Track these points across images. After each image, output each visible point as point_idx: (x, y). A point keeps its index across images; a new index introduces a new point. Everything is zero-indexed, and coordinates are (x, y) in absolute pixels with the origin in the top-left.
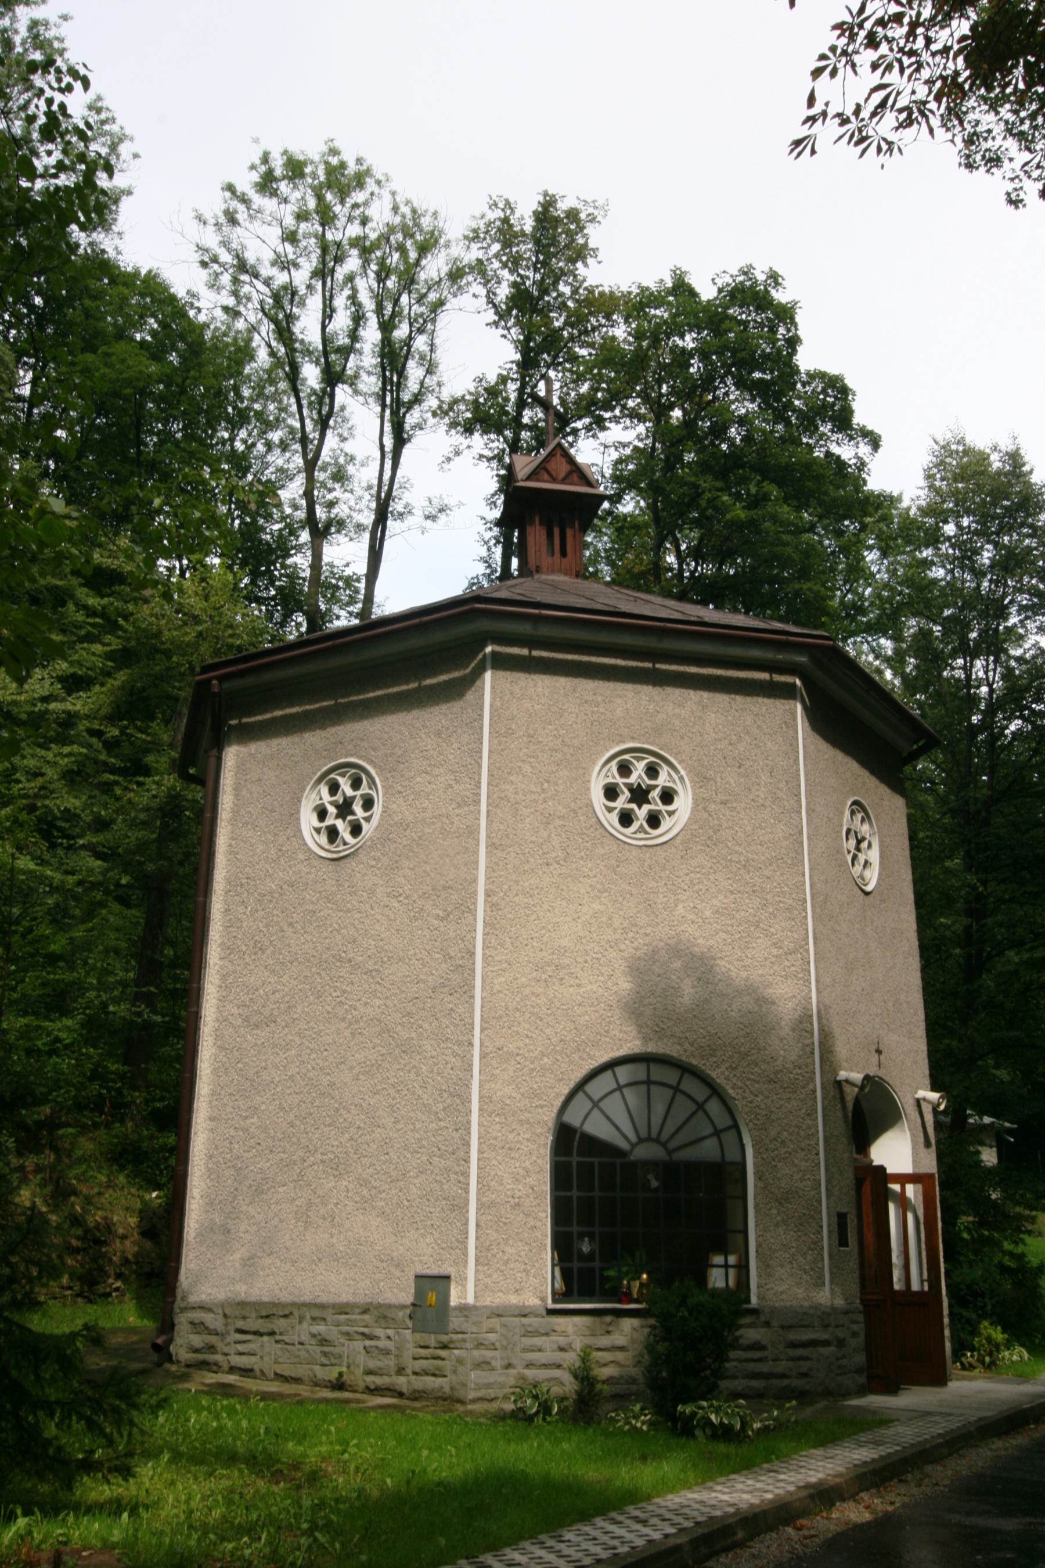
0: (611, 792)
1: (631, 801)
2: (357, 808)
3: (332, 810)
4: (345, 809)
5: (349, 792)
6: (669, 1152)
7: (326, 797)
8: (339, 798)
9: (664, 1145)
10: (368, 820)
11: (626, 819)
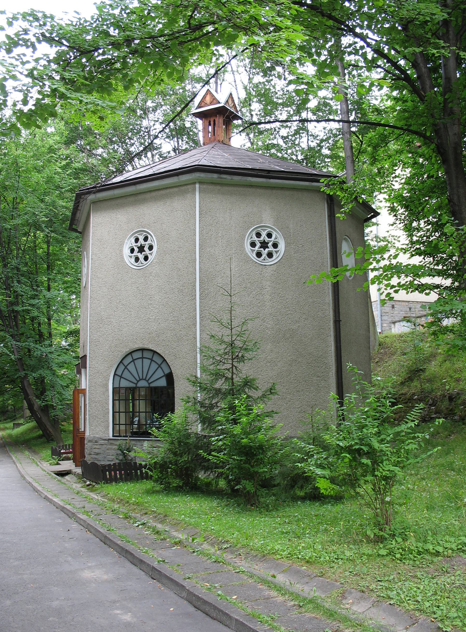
0: (253, 244)
1: (261, 247)
2: (146, 249)
3: (136, 249)
4: (141, 249)
5: (143, 243)
6: (149, 384)
7: (134, 244)
8: (139, 244)
9: (147, 381)
10: (151, 254)
11: (259, 255)
